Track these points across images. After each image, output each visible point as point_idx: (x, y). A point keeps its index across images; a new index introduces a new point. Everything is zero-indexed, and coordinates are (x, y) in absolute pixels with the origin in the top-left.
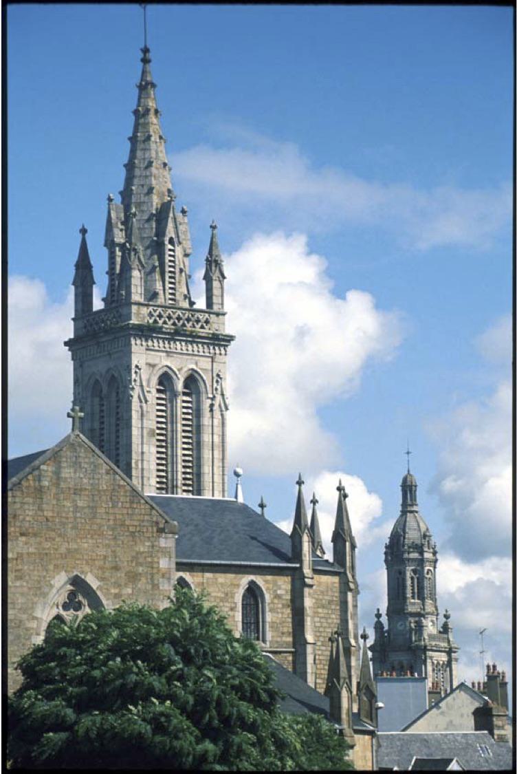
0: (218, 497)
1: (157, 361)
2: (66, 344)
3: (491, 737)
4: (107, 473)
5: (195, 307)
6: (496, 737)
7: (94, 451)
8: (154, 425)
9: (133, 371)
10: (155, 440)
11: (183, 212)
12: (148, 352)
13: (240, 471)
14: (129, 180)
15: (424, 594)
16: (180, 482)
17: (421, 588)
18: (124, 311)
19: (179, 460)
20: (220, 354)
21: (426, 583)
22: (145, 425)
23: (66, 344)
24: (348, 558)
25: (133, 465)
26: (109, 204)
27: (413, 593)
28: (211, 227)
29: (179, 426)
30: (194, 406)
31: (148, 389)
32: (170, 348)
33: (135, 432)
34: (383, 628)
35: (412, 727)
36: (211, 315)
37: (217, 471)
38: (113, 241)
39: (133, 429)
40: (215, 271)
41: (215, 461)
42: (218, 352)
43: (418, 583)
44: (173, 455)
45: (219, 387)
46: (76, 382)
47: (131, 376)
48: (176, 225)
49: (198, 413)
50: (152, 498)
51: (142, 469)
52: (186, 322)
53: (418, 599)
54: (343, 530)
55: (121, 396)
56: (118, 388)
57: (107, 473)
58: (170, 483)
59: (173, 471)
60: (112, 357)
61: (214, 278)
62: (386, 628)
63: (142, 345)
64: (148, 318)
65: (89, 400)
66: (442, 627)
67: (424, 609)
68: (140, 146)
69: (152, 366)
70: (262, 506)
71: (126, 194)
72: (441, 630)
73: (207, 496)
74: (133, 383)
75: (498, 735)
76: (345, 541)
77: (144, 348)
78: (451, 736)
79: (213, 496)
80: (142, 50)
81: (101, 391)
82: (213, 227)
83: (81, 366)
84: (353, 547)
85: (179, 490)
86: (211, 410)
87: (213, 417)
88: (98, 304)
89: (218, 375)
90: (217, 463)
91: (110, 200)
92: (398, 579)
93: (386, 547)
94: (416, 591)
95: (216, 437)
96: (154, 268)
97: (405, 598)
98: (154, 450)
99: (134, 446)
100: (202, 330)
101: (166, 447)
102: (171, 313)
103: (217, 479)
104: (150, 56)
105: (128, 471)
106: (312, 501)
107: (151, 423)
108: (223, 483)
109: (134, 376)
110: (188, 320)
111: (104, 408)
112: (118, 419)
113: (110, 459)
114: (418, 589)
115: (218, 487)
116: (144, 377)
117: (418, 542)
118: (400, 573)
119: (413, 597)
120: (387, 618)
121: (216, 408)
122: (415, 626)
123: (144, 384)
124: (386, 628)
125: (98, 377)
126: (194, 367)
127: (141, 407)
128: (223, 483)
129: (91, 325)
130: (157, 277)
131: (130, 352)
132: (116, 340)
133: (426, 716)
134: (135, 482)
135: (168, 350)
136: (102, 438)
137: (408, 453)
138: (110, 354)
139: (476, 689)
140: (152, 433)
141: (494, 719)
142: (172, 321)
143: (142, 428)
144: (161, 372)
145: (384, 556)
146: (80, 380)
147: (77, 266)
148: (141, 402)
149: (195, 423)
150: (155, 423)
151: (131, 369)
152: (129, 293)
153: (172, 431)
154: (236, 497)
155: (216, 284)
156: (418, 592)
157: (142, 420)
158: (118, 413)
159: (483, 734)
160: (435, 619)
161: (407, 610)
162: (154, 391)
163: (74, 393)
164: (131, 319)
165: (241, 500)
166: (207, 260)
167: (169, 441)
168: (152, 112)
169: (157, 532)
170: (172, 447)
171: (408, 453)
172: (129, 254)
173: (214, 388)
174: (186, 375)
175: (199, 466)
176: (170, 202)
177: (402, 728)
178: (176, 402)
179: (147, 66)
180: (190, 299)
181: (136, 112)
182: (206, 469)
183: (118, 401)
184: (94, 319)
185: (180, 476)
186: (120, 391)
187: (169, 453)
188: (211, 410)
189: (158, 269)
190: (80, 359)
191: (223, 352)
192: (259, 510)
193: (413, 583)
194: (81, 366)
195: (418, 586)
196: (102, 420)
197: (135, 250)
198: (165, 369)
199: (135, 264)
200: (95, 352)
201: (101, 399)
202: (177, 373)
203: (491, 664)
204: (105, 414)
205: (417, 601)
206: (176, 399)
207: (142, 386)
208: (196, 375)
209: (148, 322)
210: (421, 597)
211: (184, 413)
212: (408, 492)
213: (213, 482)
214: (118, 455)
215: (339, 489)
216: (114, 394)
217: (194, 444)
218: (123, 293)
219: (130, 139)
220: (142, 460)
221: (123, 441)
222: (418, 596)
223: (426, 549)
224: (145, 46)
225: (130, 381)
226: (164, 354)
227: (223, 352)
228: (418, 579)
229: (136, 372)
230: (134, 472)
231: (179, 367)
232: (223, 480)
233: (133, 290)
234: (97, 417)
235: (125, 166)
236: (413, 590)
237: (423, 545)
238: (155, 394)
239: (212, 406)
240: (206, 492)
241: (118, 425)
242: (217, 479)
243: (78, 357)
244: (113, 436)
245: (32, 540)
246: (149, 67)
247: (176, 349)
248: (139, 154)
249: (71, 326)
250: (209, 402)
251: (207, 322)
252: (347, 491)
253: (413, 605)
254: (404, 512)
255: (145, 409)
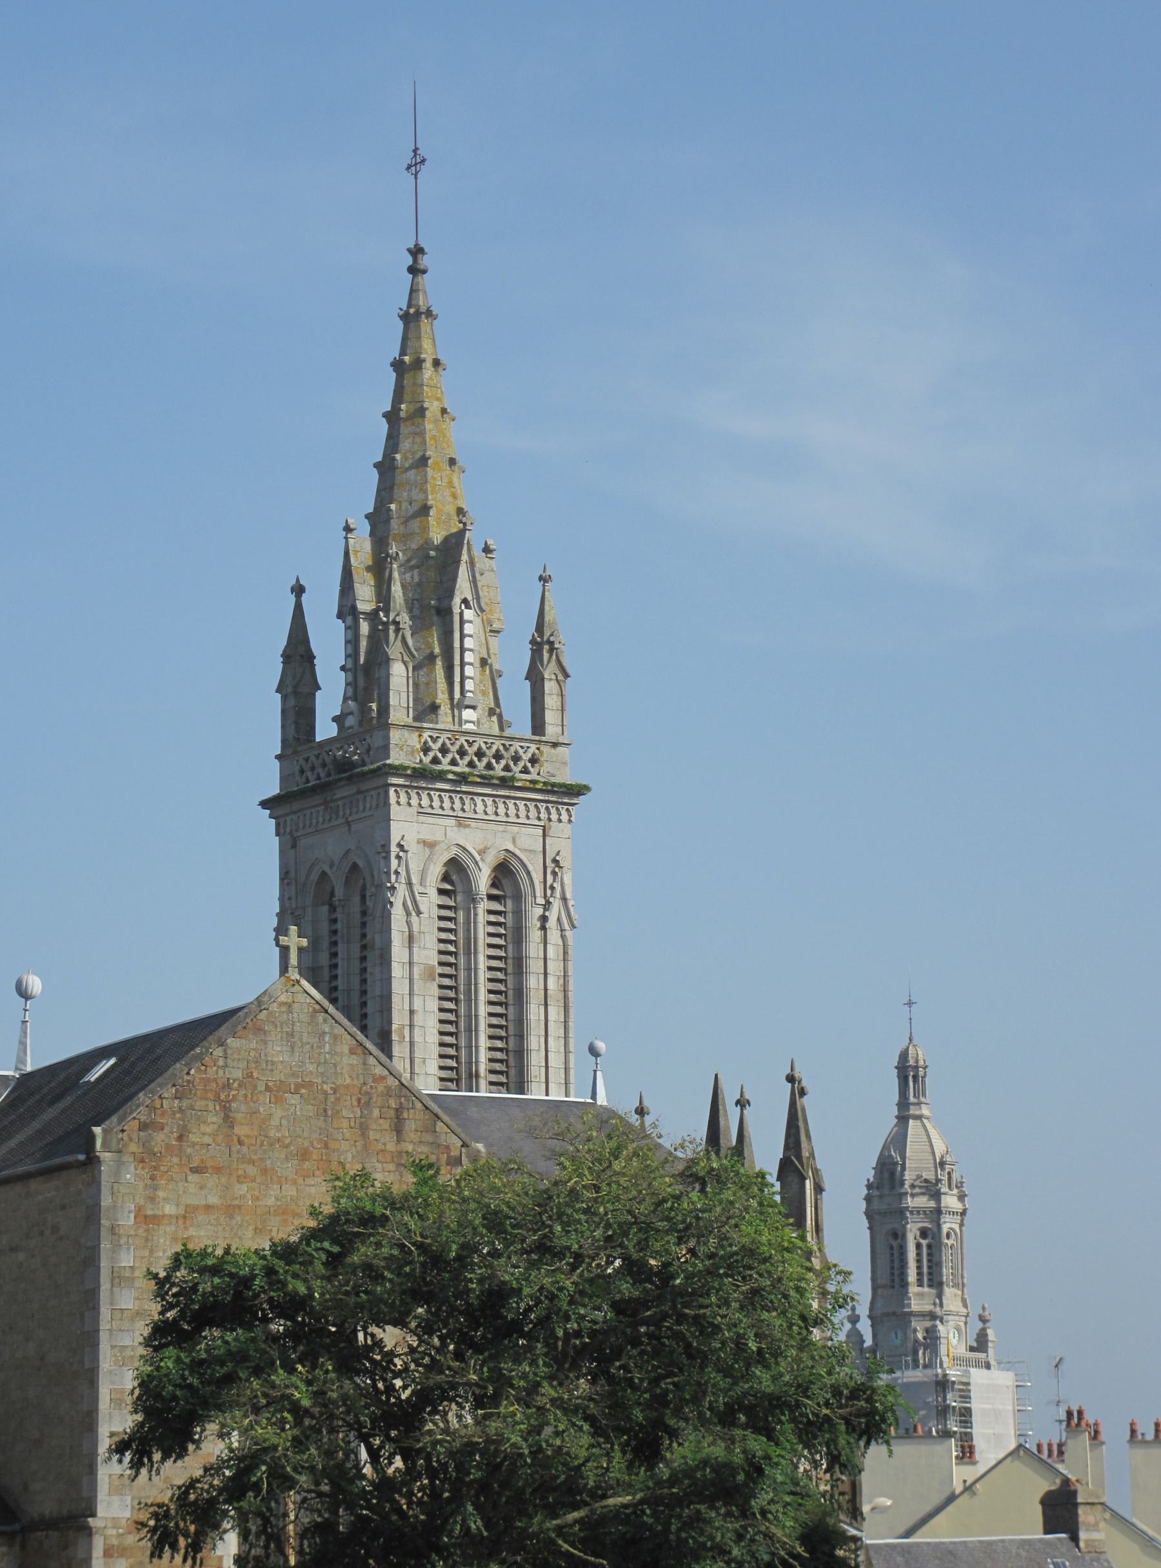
0: (556, 1095)
1: (438, 836)
2: (264, 804)
3: (1072, 1544)
4: (352, 1052)
5: (508, 732)
6: (1082, 1544)
7: (326, 1012)
8: (433, 959)
9: (393, 855)
10: (436, 986)
11: (487, 550)
12: (422, 818)
13: (601, 1046)
14: (385, 492)
15: (941, 1275)
16: (483, 1069)
17: (935, 1265)
18: (376, 741)
19: (482, 1026)
20: (560, 821)
21: (946, 1257)
22: (416, 959)
23: (264, 804)
24: (808, 1204)
25: (395, 1037)
26: (346, 538)
27: (920, 1274)
28: (541, 578)
29: (481, 958)
30: (509, 920)
31: (422, 890)
32: (463, 810)
33: (398, 971)
34: (864, 1341)
35: (925, 1529)
36: (542, 748)
37: (555, 1045)
38: (354, 608)
39: (394, 965)
40: (549, 661)
41: (551, 1025)
42: (554, 816)
43: (929, 1254)
44: (470, 1016)
45: (557, 885)
46: (285, 876)
47: (389, 866)
48: (474, 577)
49: (518, 936)
50: (432, 1097)
51: (412, 1044)
52: (493, 761)
53: (930, 1286)
54: (799, 1157)
55: (369, 903)
56: (364, 888)
57: (352, 1052)
58: (463, 1069)
59: (469, 1047)
60: (353, 828)
61: (546, 676)
62: (868, 1342)
63: (409, 804)
64: (422, 754)
65: (309, 911)
66: (977, 1340)
67: (941, 1305)
68: (405, 429)
69: (430, 845)
70: (641, 1111)
71: (378, 519)
72: (975, 1344)
73: (536, 1093)
74: (393, 877)
75: (1086, 1541)
76: (803, 1179)
77: (415, 809)
78: (1000, 1544)
79: (547, 1095)
80: (409, 250)
81: (332, 894)
82: (544, 579)
83: (294, 846)
84: (819, 1189)
85: (483, 1083)
86: (543, 928)
87: (545, 943)
88: (325, 730)
89: (555, 861)
90: (556, 1030)
91: (348, 529)
92: (892, 1248)
93: (869, 1186)
94: (925, 1270)
95: (551, 982)
96: (431, 658)
97: (904, 1285)
98: (433, 1005)
99: (395, 999)
100: (524, 776)
101: (456, 1000)
102: (465, 744)
103: (556, 1061)
104: (425, 261)
105: (385, 1042)
106: (738, 1102)
107: (428, 953)
108: (567, 1070)
109: (394, 863)
110: (498, 756)
111: (339, 926)
112: (364, 947)
113: (350, 1020)
114: (929, 1267)
115: (556, 1076)
116: (415, 867)
117: (929, 1175)
118: (895, 1235)
119: (920, 1283)
120: (869, 1322)
121: (552, 923)
122: (925, 1338)
123: (415, 880)
124: (868, 1342)
125: (327, 869)
126: (511, 848)
127: (409, 924)
128: (567, 1070)
129: (313, 769)
130: (439, 665)
131: (388, 819)
132: (360, 797)
133: (950, 1508)
134: (400, 1063)
135: (460, 814)
136: (334, 984)
137: (910, 1004)
138: (348, 823)
139: (1045, 1456)
140: (429, 975)
141: (1080, 1511)
142: (467, 759)
143: (411, 963)
144: (446, 857)
145: (864, 1205)
146: (292, 874)
147: (287, 657)
148: (408, 914)
149: (510, 954)
150: (436, 953)
151: (388, 852)
152: (384, 709)
153: (469, 969)
154: (594, 1095)
155: (550, 686)
156: (930, 1274)
157: (410, 947)
158: (364, 936)
159: (1058, 1539)
160: (962, 1324)
161: (909, 1305)
162: (433, 893)
163: (281, 899)
164: (388, 757)
165: (602, 1100)
166: (533, 642)
167: (462, 988)
168: (428, 364)
169: (448, 1164)
170: (469, 1000)
171: (910, 1004)
172: (386, 631)
173: (548, 884)
174: (494, 863)
175: (521, 1036)
176: (462, 533)
177: (902, 1529)
178: (476, 915)
179: (419, 278)
180: (500, 717)
181: (398, 365)
182: (534, 1042)
183: (364, 913)
184: (317, 757)
185: (483, 1056)
186: (368, 894)
187: (462, 1011)
188: (543, 928)
189: (439, 663)
190: (291, 833)
191: (565, 817)
192: (634, 1119)
193: (919, 1254)
194: (294, 846)
195: (929, 1261)
196: (333, 950)
197: (397, 623)
198: (454, 851)
199: (394, 649)
200: (321, 820)
201: (333, 909)
202: (478, 858)
203: (1075, 1409)
204: (338, 938)
205: (926, 1289)
206: (475, 908)
207: (410, 884)
208: (515, 863)
209: (421, 761)
210: (936, 1283)
211: (490, 935)
212: (911, 1079)
213: (547, 1067)
214: (364, 1016)
215: (791, 1079)
216: (357, 899)
217: (510, 993)
218: (374, 706)
219: (386, 415)
220: (411, 1026)
221: (374, 989)
222: (930, 1280)
223: (944, 1189)
224: (416, 245)
225: (388, 873)
226: (452, 822)
227: (565, 817)
228: (929, 1246)
229: (398, 857)
230: (396, 1050)
231: (481, 847)
232: (566, 1062)
233: (393, 701)
234: (325, 944)
235: (377, 465)
236: (919, 1268)
237: (938, 1181)
238: (435, 898)
239: (544, 919)
240: (534, 1086)
241: (363, 959)
242: (556, 1061)
243: (288, 830)
244: (356, 981)
245: (211, 1180)
246: (425, 280)
247: (476, 812)
248: (405, 444)
249: (274, 770)
250: (539, 911)
251: (534, 761)
252: (804, 1084)
253: (918, 1299)
254: (903, 1119)
255: (415, 929)
